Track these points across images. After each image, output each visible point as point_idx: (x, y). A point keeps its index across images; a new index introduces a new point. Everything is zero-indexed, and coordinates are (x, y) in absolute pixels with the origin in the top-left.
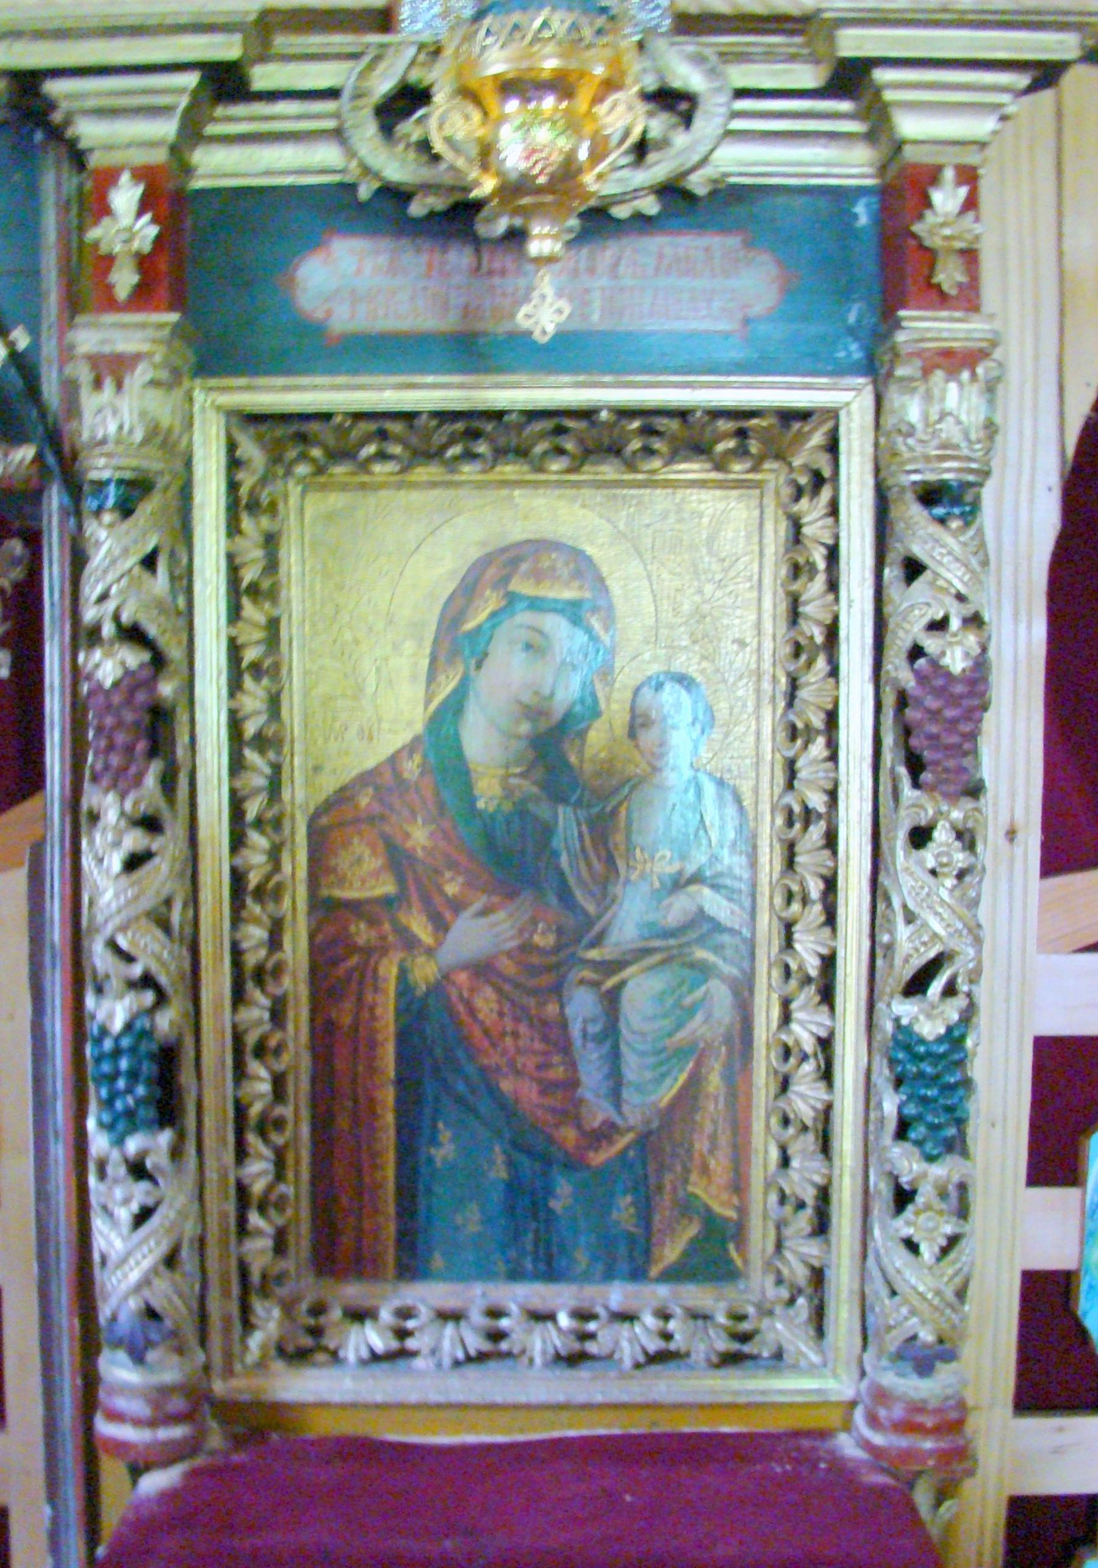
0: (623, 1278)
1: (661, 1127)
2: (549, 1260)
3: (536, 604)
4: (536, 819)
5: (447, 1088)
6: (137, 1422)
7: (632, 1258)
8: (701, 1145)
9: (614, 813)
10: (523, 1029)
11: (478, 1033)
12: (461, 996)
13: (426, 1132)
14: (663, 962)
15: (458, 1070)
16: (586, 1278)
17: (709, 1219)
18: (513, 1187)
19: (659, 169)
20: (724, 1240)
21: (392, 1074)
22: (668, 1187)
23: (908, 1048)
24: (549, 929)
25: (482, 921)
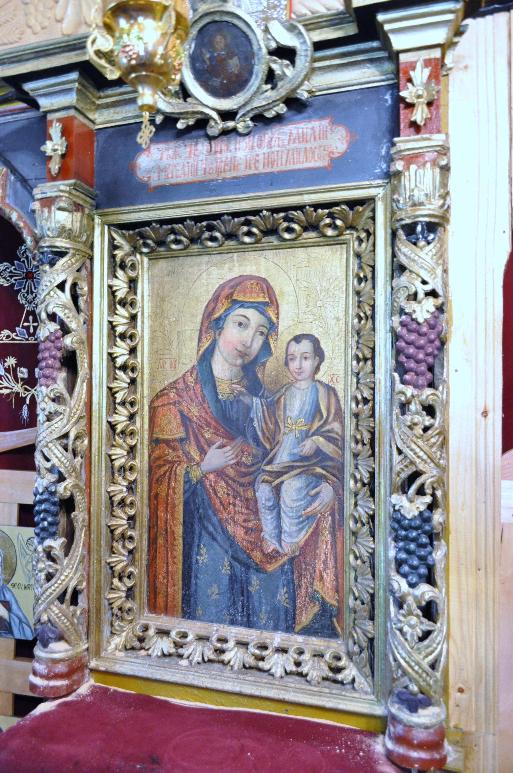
0: (282, 630)
1: (300, 555)
3: (243, 305)
4: (244, 404)
5: (206, 529)
6: (42, 676)
7: (286, 621)
8: (320, 566)
10: (237, 502)
11: (218, 502)
12: (211, 485)
13: (196, 548)
14: (300, 473)
15: (210, 521)
16: (265, 628)
17: (324, 604)
18: (233, 578)
19: (283, 89)
20: (331, 616)
22: (304, 586)
23: (398, 522)
24: (249, 455)
25: (220, 450)
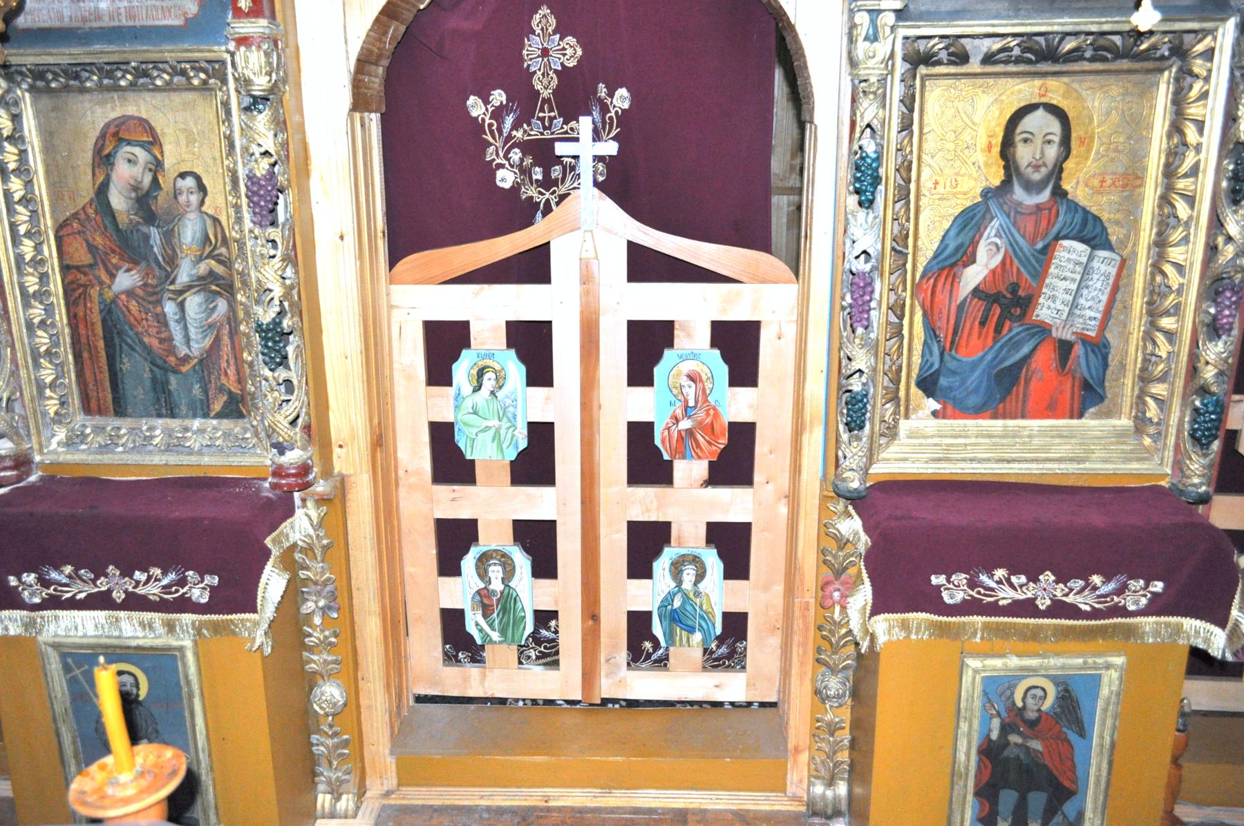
2: (171, 409)
7: (202, 409)
8: (224, 365)
9: (173, 230)
16: (187, 417)
18: (154, 380)
21: (101, 335)
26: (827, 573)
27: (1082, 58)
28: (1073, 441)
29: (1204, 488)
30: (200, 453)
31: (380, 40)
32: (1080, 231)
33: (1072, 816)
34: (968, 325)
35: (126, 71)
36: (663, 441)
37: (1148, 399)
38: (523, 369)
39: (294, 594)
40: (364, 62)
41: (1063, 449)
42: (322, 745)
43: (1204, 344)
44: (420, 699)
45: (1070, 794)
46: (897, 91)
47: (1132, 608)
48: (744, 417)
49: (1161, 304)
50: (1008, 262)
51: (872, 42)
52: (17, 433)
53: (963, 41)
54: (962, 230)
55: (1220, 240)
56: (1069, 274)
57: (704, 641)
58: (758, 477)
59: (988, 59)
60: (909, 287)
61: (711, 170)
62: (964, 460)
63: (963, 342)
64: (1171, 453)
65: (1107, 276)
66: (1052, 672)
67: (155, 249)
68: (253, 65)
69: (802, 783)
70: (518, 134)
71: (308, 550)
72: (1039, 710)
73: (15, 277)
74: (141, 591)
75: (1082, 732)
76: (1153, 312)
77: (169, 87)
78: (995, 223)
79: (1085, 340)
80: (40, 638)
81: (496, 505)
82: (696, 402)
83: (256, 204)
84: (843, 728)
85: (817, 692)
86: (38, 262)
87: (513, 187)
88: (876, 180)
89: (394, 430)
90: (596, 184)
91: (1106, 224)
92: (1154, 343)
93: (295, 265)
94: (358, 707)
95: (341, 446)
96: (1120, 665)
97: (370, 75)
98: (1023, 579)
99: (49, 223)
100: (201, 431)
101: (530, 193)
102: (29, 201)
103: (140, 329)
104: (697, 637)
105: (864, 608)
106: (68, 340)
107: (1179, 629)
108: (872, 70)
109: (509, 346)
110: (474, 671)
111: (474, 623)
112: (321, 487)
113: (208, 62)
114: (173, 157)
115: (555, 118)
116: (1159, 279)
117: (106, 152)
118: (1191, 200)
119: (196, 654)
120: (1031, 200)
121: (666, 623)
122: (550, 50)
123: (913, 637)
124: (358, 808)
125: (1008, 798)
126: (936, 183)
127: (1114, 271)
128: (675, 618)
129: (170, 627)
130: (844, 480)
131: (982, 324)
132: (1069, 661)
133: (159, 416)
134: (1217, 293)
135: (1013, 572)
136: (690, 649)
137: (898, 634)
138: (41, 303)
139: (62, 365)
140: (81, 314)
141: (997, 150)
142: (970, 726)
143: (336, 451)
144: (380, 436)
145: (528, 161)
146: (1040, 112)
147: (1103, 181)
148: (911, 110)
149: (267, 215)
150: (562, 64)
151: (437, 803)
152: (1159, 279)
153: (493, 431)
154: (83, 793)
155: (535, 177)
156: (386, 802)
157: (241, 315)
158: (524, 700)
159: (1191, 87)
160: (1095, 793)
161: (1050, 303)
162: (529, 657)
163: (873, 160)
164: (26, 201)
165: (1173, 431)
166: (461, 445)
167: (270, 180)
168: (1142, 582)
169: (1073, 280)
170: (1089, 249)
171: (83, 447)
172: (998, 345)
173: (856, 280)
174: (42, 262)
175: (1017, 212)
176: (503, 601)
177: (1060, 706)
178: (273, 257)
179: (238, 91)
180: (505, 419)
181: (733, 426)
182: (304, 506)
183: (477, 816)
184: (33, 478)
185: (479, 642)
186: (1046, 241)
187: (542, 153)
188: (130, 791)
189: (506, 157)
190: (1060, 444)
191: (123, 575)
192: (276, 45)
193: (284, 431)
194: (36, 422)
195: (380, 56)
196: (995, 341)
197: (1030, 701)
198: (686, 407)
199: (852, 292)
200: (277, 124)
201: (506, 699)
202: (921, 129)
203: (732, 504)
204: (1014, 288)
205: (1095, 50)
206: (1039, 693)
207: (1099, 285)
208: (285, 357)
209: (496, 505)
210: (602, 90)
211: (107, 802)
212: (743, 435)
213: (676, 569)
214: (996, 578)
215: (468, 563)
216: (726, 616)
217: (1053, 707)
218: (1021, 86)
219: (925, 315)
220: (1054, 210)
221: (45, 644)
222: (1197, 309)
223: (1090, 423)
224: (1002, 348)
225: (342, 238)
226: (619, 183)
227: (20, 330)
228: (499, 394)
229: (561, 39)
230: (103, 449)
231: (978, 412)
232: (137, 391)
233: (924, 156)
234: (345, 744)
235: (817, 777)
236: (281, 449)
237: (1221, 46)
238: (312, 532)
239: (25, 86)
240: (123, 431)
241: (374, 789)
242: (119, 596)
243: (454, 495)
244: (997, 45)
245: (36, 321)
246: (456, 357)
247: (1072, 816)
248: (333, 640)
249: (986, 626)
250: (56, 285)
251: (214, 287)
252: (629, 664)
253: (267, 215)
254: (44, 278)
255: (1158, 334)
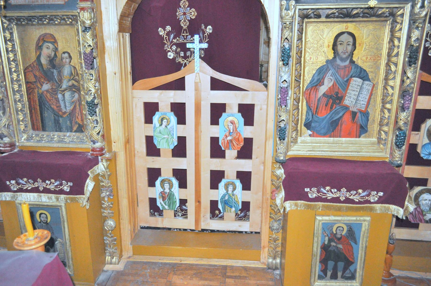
2: (60, 129)
6: (3, 147)
8: (77, 115)
9: (61, 71)
16: (65, 132)
17: (79, 124)
18: (55, 119)
26: (274, 188)
27: (359, 16)
28: (356, 145)
29: (399, 162)
30: (69, 143)
31: (129, 9)
32: (359, 75)
33: (353, 270)
34: (321, 106)
35: (46, 19)
36: (222, 144)
37: (382, 132)
38: (176, 118)
39: (97, 189)
40: (123, 17)
41: (353, 148)
42: (108, 240)
43: (400, 113)
44: (142, 228)
45: (352, 263)
46: (296, 27)
47: (372, 201)
48: (249, 136)
49: (386, 99)
50: (335, 84)
51: (287, 10)
52: (11, 136)
53: (320, 10)
54: (319, 74)
55: (405, 78)
56: (355, 89)
57: (236, 211)
58: (253, 156)
59: (328, 16)
60: (301, 93)
61: (238, 53)
62: (319, 151)
63: (320, 112)
64: (389, 150)
65: (368, 90)
66: (345, 222)
67: (55, 77)
68: (86, 17)
69: (265, 258)
70: (175, 41)
71: (103, 176)
72: (341, 235)
73: (11, 85)
74: (48, 187)
75: (356, 243)
76: (384, 102)
77: (59, 24)
78: (330, 72)
79: (361, 112)
80: (17, 202)
81: (167, 164)
82: (233, 131)
83: (86, 62)
84: (278, 240)
85: (270, 228)
86: (18, 80)
87: (173, 58)
88: (289, 57)
89: (134, 138)
90: (200, 57)
91: (368, 72)
92: (384, 113)
93: (99, 82)
94: (120, 229)
95: (115, 142)
96: (370, 221)
97: (125, 20)
98: (336, 190)
99: (22, 68)
100: (69, 136)
101: (179, 60)
102: (15, 61)
103: (50, 103)
104: (233, 209)
105: (282, 198)
106: (28, 106)
107: (388, 209)
108: (288, 20)
109: (172, 111)
110: (159, 218)
111: (159, 203)
112: (107, 155)
113: (72, 16)
114: (61, 47)
115: (188, 35)
116: (385, 91)
117: (40, 45)
118: (396, 65)
119: (66, 208)
120: (343, 64)
121: (223, 204)
122: (186, 13)
123: (299, 209)
124: (119, 262)
125: (331, 264)
126: (311, 58)
127: (371, 88)
128: (226, 203)
129: (57, 199)
130: (278, 157)
131: (326, 105)
132: (352, 219)
133: (56, 131)
134: (404, 96)
135: (332, 187)
136: (231, 213)
137: (294, 208)
138: (19, 94)
139: (25, 114)
140: (32, 98)
141: (331, 47)
142: (318, 239)
143: (113, 144)
144: (128, 139)
145: (179, 50)
146: (346, 35)
147: (367, 58)
148: (302, 34)
149: (90, 65)
150: (190, 18)
151: (145, 261)
152: (385, 91)
153: (166, 139)
154: (18, 243)
155: (181, 55)
156: (129, 260)
157: (82, 99)
158: (177, 229)
159: (396, 26)
160: (360, 263)
161: (349, 99)
162: (179, 215)
163: (288, 50)
164: (14, 60)
165: (389, 143)
166: (156, 143)
167: (91, 54)
168: (376, 192)
169: (357, 91)
170: (362, 81)
171: (32, 141)
172: (332, 112)
173: (282, 90)
174: (19, 81)
175: (338, 68)
176: (169, 196)
177: (349, 234)
178: (92, 79)
179: (81, 25)
180: (170, 135)
181: (245, 139)
182: (102, 161)
183: (158, 265)
184: (16, 151)
185: (161, 209)
186: (348, 78)
187: (182, 47)
188: (33, 242)
189: (171, 48)
190: (352, 146)
191: (43, 182)
192: (93, 10)
193: (95, 137)
194: (17, 132)
195: (129, 15)
196: (331, 111)
197: (338, 231)
198: (230, 132)
199: (281, 94)
200: (94, 36)
201: (171, 228)
202: (305, 40)
203: (245, 165)
204: (337, 93)
205: (363, 14)
206: (341, 229)
207: (365, 93)
208: (96, 112)
209: (167, 164)
210: (203, 27)
211: (25, 245)
212: (249, 142)
213: (226, 186)
214: (326, 190)
215: (158, 183)
216: (243, 203)
217: (346, 234)
218: (339, 26)
219: (307, 102)
220: (350, 68)
221: (18, 203)
222: (398, 101)
223: (363, 139)
224: (333, 114)
225: (115, 74)
226: (208, 57)
227: (12, 102)
228: (168, 127)
229: (190, 9)
230: (38, 141)
231: (324, 135)
232: (50, 123)
233: (306, 49)
234: (115, 240)
235: (270, 256)
236: (94, 143)
237: (406, 12)
238: (104, 169)
239: (14, 23)
240: (44, 136)
241: (125, 255)
242: (41, 189)
243: (154, 160)
244: (331, 12)
245: (17, 99)
246: (154, 114)
247: (353, 270)
248: (111, 206)
249: (323, 206)
250: (24, 88)
251: (74, 90)
252: (211, 218)
253: (90, 65)
254: (20, 86)
255: (385, 110)
